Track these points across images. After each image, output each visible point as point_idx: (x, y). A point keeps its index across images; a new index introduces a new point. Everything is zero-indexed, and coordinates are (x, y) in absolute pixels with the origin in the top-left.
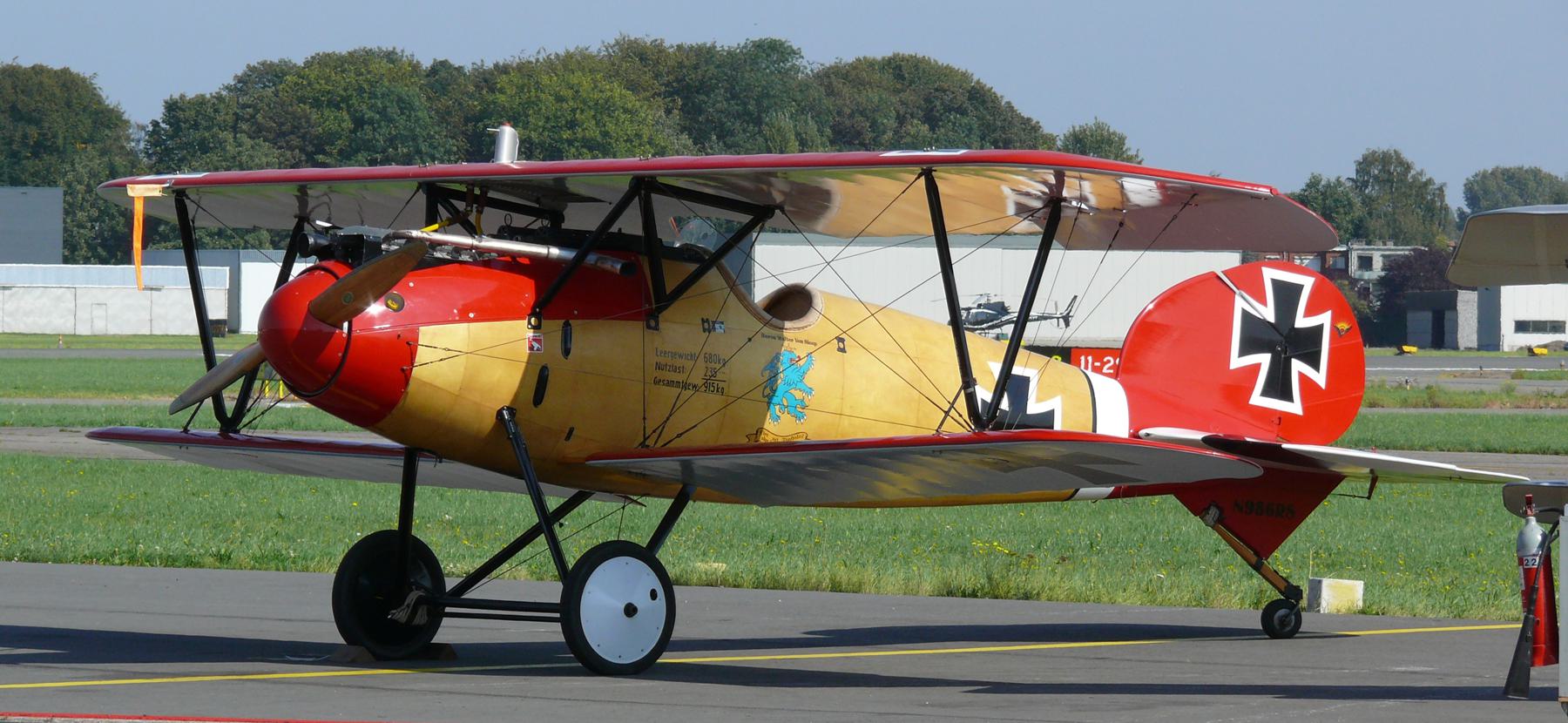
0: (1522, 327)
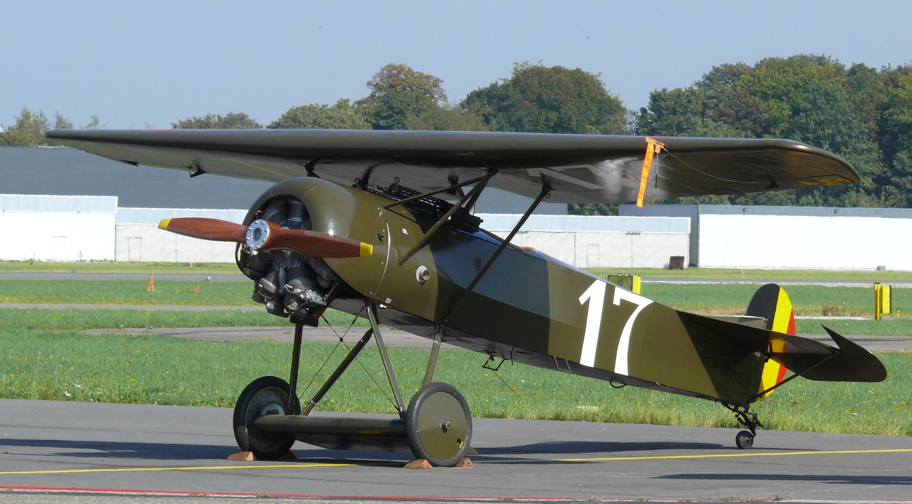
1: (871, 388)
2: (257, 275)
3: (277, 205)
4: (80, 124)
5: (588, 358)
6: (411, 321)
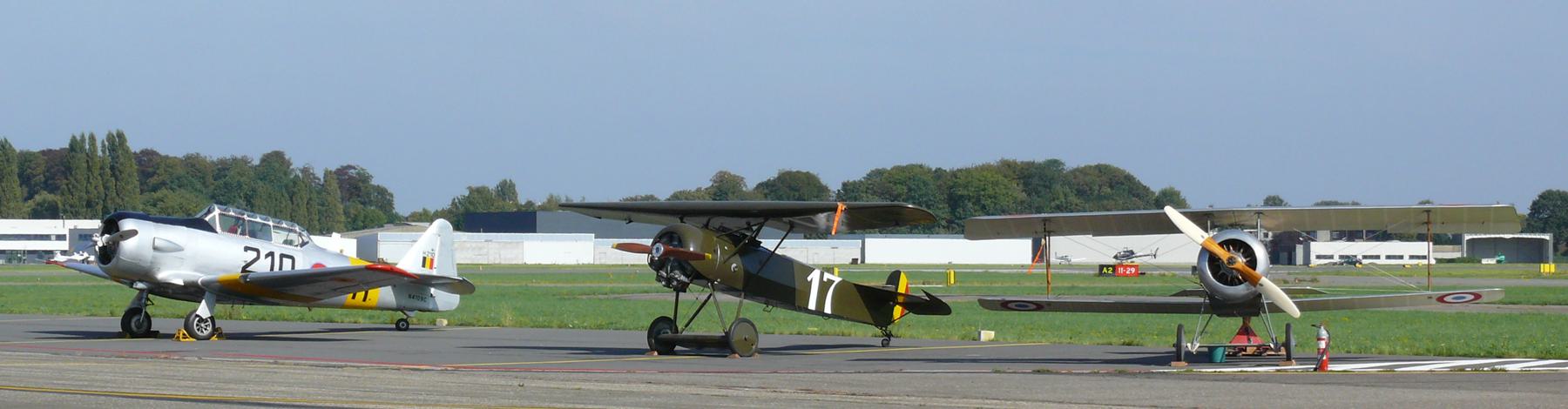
0: (1318, 257)
1: (944, 318)
2: (657, 270)
3: (667, 236)
4: (577, 200)
5: (812, 306)
6: (730, 289)
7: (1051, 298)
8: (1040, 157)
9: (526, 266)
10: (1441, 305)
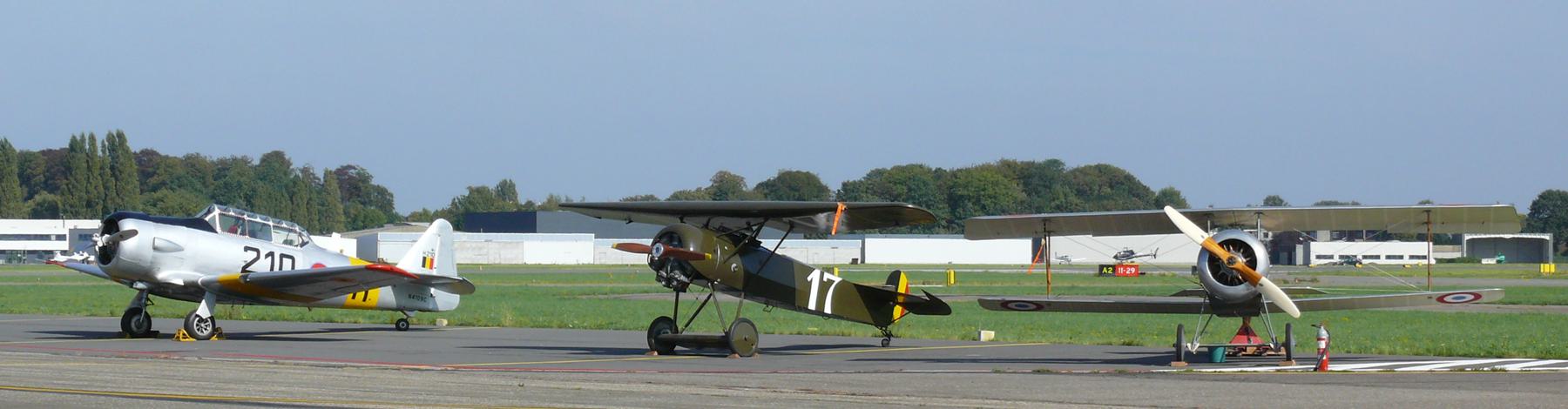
0: (1318, 257)
7: (1051, 298)
8: (1040, 157)
9: (526, 266)
10: (1441, 305)
